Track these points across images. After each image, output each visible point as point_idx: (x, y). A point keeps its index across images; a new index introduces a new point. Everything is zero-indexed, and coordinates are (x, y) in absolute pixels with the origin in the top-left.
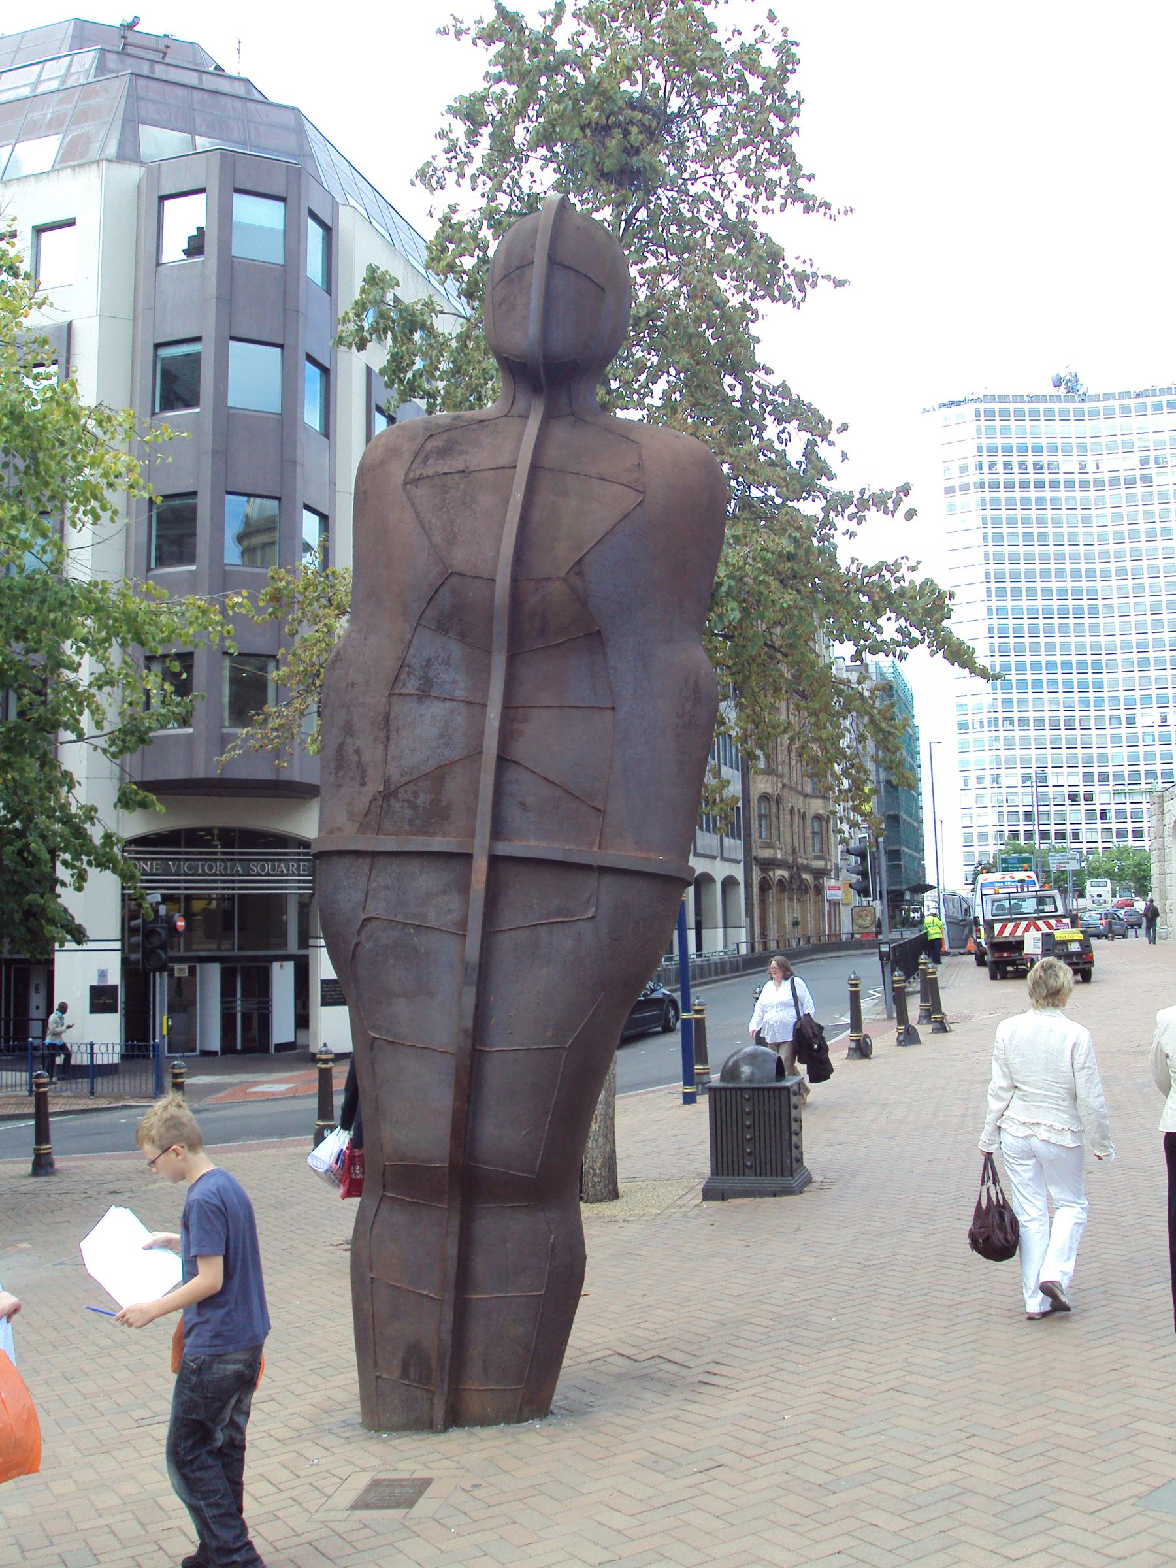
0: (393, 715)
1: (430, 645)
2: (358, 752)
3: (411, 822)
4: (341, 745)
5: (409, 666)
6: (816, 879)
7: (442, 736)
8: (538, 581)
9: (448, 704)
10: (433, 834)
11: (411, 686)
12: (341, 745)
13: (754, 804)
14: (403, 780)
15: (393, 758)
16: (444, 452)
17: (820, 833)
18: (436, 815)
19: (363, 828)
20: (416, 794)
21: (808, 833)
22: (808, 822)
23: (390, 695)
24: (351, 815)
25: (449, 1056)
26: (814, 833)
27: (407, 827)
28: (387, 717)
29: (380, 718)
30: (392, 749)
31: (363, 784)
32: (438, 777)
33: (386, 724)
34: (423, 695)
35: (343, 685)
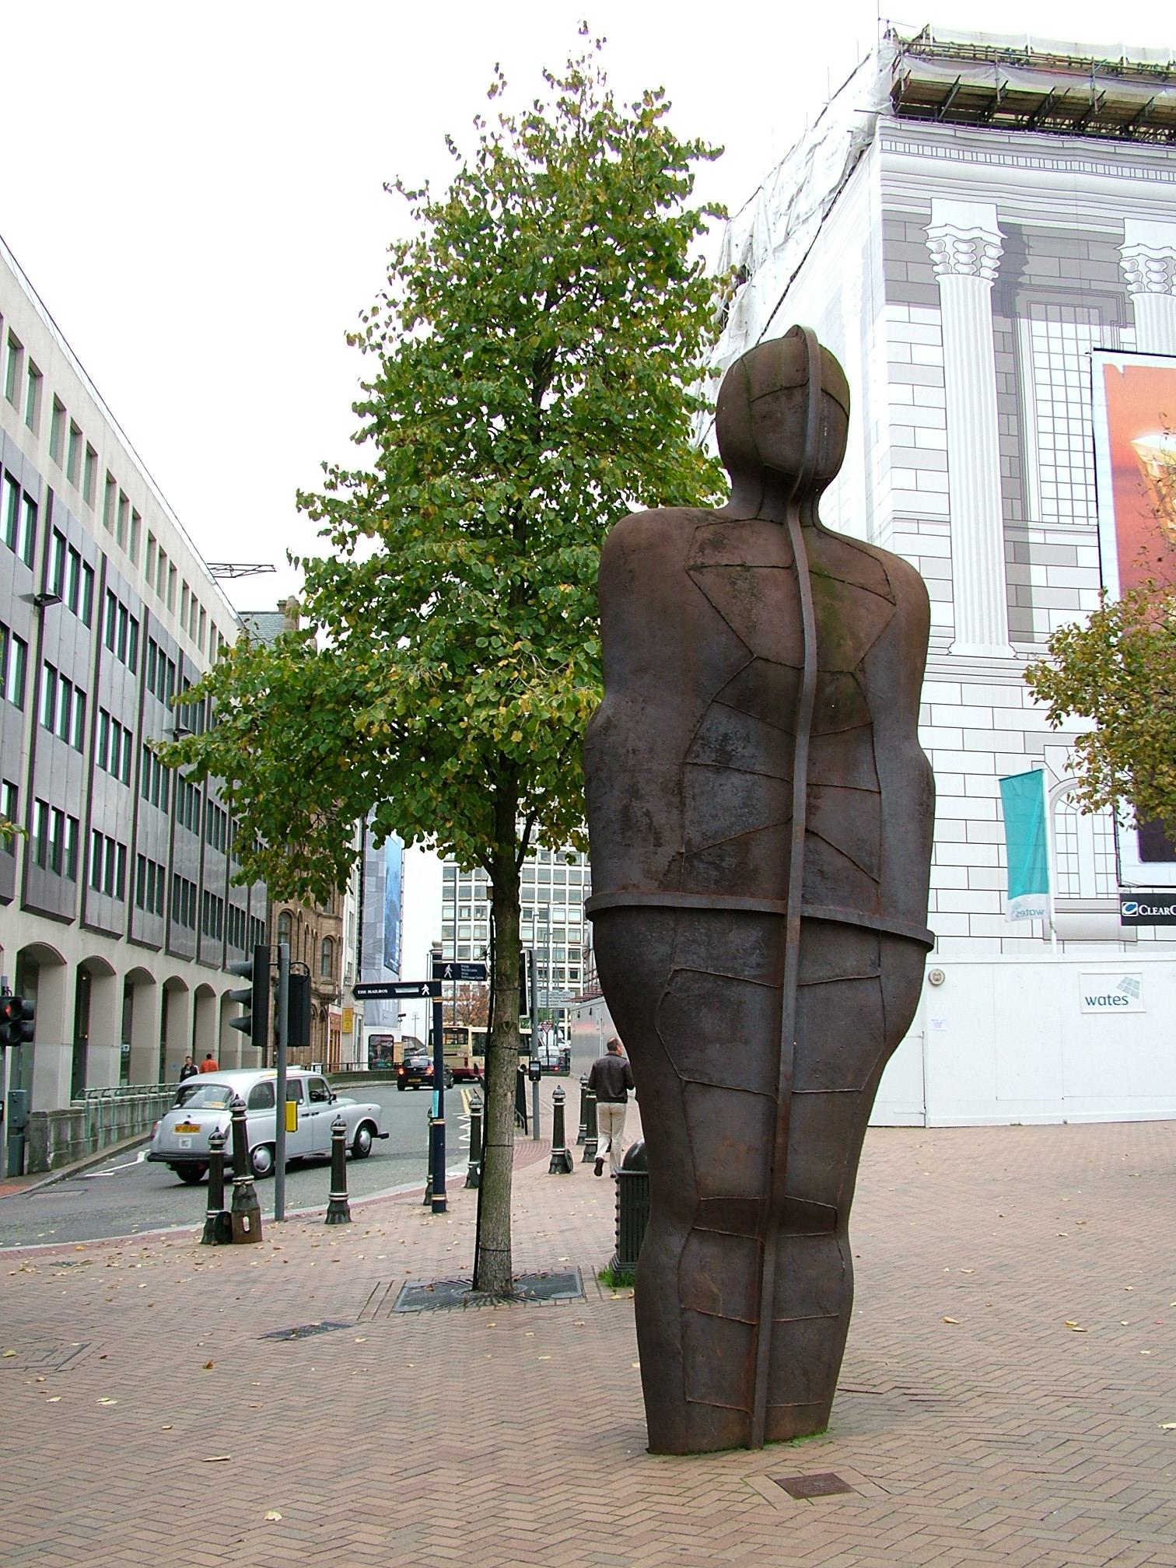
0: (686, 783)
1: (722, 722)
2: (648, 814)
3: (716, 882)
4: (626, 807)
5: (702, 738)
6: (322, 1005)
7: (745, 805)
8: (833, 673)
9: (749, 777)
10: (742, 894)
11: (708, 757)
12: (626, 807)
13: (275, 920)
14: (706, 844)
15: (692, 822)
16: (717, 544)
17: (330, 956)
18: (740, 879)
19: (665, 886)
20: (721, 857)
21: (319, 956)
22: (319, 944)
23: (684, 764)
24: (648, 874)
25: (751, 1098)
26: (323, 956)
27: (713, 887)
28: (680, 783)
29: (672, 785)
30: (690, 815)
31: (658, 845)
32: (743, 843)
33: (678, 790)
34: (724, 764)
35: (622, 751)
